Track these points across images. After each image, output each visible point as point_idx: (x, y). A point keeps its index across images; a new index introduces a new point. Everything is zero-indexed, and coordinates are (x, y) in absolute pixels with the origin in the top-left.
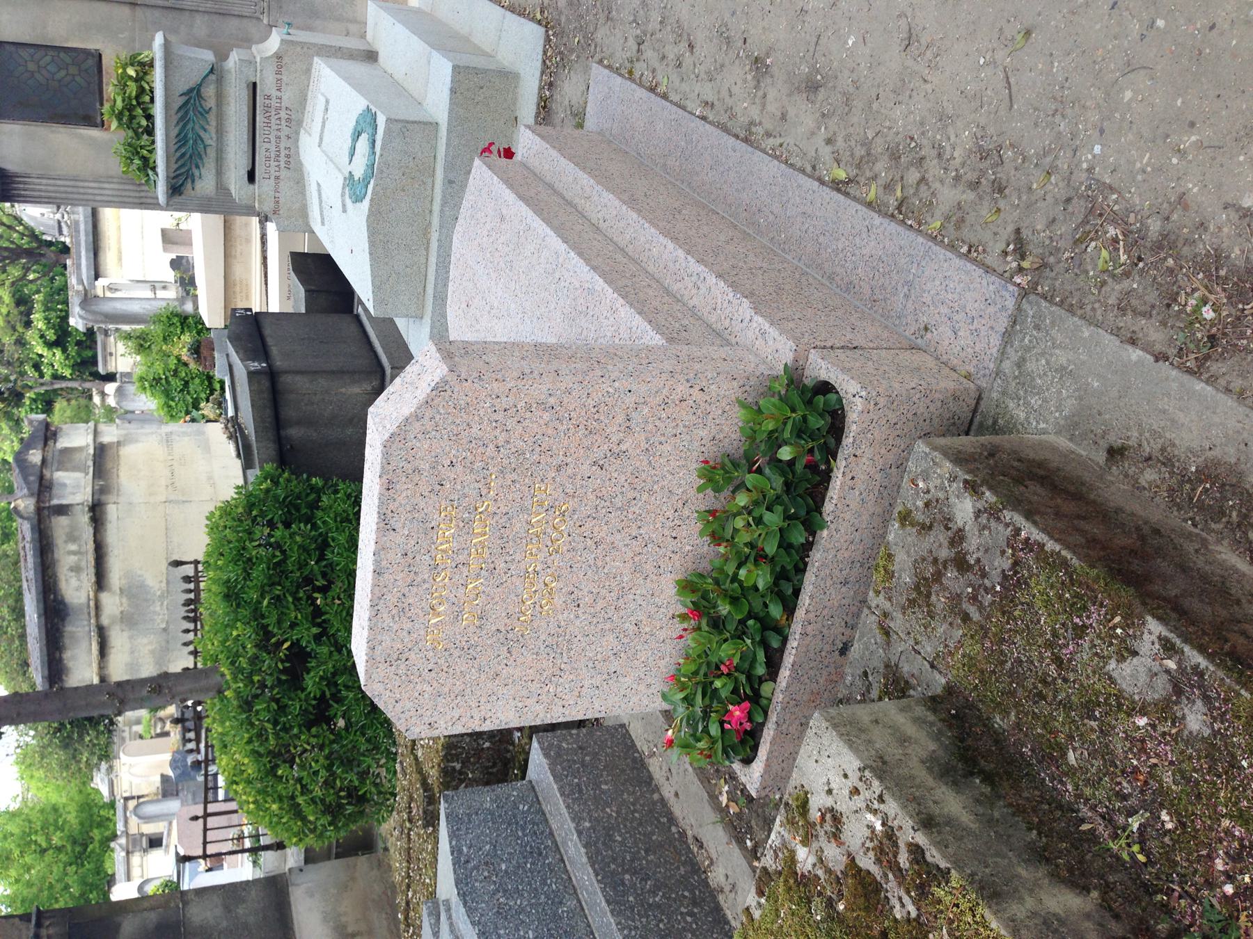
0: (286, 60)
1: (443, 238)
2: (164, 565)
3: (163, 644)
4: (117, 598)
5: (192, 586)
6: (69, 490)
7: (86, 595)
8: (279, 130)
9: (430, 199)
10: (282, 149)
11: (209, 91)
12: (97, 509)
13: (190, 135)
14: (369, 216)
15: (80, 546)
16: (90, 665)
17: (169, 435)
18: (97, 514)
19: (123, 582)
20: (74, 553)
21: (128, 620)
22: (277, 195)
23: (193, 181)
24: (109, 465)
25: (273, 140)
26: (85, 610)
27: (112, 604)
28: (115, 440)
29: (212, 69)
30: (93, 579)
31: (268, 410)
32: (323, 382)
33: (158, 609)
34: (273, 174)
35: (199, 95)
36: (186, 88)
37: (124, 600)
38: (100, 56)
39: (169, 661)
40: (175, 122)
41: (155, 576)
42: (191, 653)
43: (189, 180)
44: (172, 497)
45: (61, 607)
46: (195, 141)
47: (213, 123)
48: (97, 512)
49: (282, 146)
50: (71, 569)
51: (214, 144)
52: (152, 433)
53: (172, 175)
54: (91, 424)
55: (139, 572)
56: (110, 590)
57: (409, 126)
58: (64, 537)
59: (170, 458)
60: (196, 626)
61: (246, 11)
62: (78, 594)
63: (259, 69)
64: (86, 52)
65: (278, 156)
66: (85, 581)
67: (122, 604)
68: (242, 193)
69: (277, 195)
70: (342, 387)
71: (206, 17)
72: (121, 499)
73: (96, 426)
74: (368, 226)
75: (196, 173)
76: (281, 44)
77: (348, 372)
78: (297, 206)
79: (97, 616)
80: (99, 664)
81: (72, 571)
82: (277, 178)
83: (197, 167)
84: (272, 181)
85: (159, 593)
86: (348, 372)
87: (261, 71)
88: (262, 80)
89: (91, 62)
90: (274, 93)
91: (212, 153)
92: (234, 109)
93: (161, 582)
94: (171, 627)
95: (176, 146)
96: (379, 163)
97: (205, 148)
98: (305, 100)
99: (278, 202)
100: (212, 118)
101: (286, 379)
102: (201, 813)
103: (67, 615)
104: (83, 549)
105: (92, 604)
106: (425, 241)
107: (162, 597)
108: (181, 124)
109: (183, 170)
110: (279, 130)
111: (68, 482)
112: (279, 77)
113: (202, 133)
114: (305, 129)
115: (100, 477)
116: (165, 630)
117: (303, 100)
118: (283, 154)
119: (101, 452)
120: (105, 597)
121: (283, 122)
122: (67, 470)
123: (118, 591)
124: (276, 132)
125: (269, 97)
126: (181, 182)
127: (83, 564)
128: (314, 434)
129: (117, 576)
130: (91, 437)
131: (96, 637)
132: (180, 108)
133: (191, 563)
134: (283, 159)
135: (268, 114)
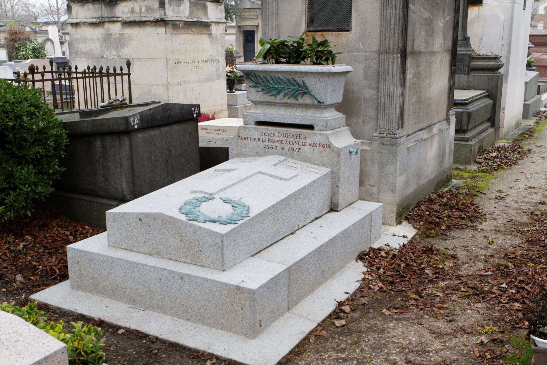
0: (328, 150)
1: (148, 268)
2: (128, 57)
3: (96, 56)
4: (118, 32)
5: (118, 71)
6: (176, 8)
7: (120, 16)
8: (286, 143)
9: (178, 259)
10: (276, 144)
11: (307, 100)
12: (163, 23)
13: (280, 86)
14: (163, 214)
15: (144, 13)
16: (86, 18)
17: (217, 61)
18: (160, 23)
19: (126, 35)
20: (140, 10)
21: (107, 37)
22: (249, 139)
23: (254, 87)
24: (194, 29)
25: (281, 139)
26: (112, 16)
27: (116, 28)
28: (213, 32)
29: (320, 102)
30: (127, 20)
31: (107, 128)
32: (126, 163)
33: (113, 53)
34: (261, 137)
35: (304, 93)
36: (308, 85)
37: (117, 36)
38: (348, 31)
39: (87, 58)
40: (287, 77)
41: (127, 52)
42: (85, 70)
43: (254, 84)
44: (170, 62)
45: (114, 3)
46: (276, 89)
47: (289, 101)
48: (162, 22)
49: (277, 144)
50: (132, 9)
51: (277, 101)
52: (218, 52)
53: (256, 74)
54: (224, 20)
55: (131, 44)
56: (122, 28)
57: (220, 251)
58: (148, 5)
59: (200, 61)
60: (98, 73)
61: (381, 123)
62: (120, 12)
63: (322, 132)
64: (349, 23)
65: (271, 141)
66: (126, 16)
67: (115, 34)
68: (249, 117)
69: (249, 139)
70: (125, 175)
71: (375, 97)
72: (169, 36)
73: (223, 23)
74: (157, 214)
75: (259, 89)
76: (338, 148)
77: (133, 180)
78: (244, 151)
79: (109, 22)
80: (86, 22)
81: (132, 9)
82: (259, 140)
83: (263, 90)
84: (256, 136)
85: (121, 54)
86: (133, 180)
87: (320, 134)
88: (315, 134)
89: (344, 26)
90: (308, 141)
91: (272, 99)
92: (299, 114)
93: (126, 55)
94: (104, 60)
95: (273, 77)
96: (195, 226)
97: (274, 95)
98: (305, 161)
99: (245, 139)
100: (292, 101)
101: (126, 141)
102: (78, 71)
103: (110, 6)
104: (142, 15)
105: (115, 19)
106: (152, 253)
107: (119, 55)
108: (286, 81)
109: (260, 81)
110: (286, 143)
111: (182, 7)
112: (318, 145)
113: (282, 94)
114: (285, 160)
115: (185, 24)
116: (102, 57)
117: (304, 159)
118: (273, 144)
119: (206, 25)
120: (119, 25)
121: (291, 146)
122: (190, 7)
123: (121, 33)
124: (285, 141)
125: (305, 138)
126: (253, 79)
127: (135, 15)
128: (98, 156)
129: (129, 33)
130: (215, 20)
131: (99, 21)
132: (295, 81)
133: (129, 71)
134: (270, 144)
135: (295, 137)
